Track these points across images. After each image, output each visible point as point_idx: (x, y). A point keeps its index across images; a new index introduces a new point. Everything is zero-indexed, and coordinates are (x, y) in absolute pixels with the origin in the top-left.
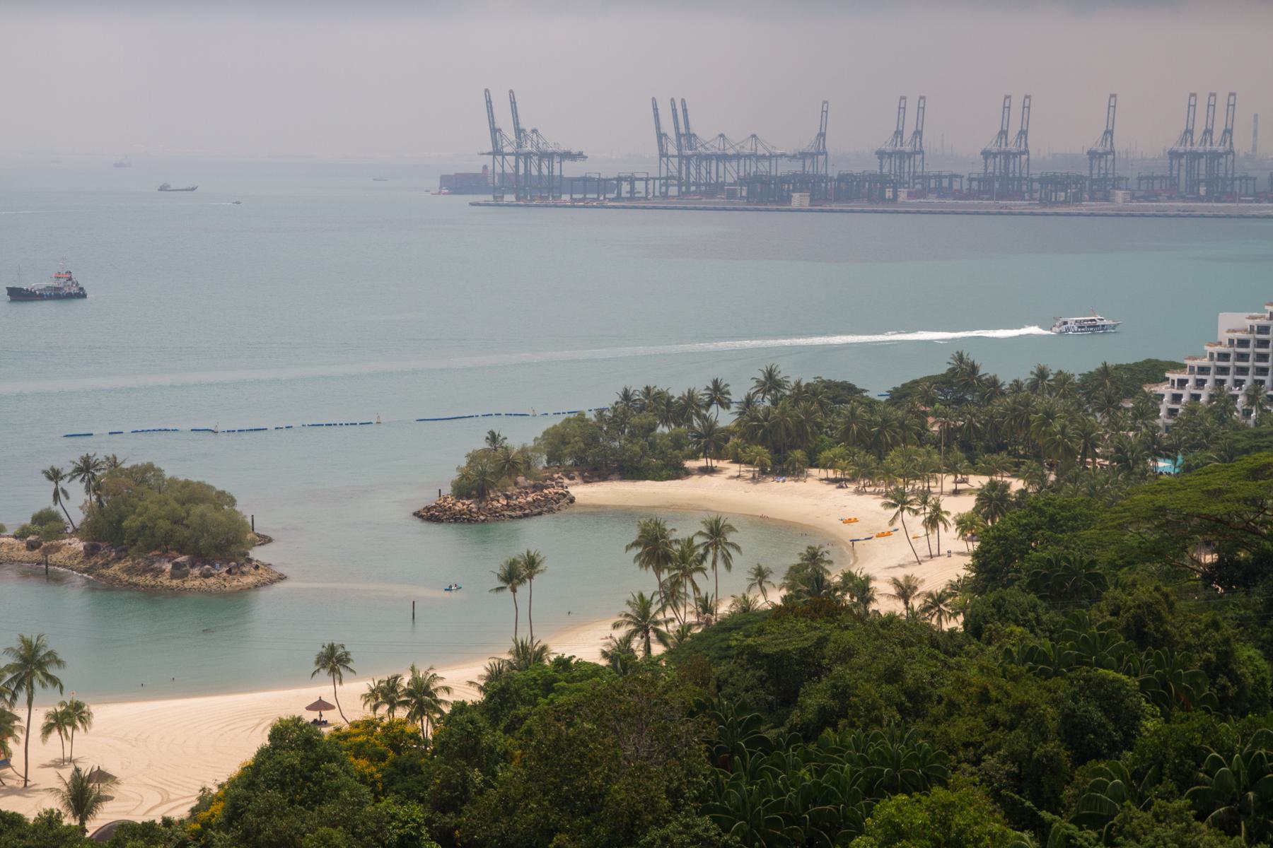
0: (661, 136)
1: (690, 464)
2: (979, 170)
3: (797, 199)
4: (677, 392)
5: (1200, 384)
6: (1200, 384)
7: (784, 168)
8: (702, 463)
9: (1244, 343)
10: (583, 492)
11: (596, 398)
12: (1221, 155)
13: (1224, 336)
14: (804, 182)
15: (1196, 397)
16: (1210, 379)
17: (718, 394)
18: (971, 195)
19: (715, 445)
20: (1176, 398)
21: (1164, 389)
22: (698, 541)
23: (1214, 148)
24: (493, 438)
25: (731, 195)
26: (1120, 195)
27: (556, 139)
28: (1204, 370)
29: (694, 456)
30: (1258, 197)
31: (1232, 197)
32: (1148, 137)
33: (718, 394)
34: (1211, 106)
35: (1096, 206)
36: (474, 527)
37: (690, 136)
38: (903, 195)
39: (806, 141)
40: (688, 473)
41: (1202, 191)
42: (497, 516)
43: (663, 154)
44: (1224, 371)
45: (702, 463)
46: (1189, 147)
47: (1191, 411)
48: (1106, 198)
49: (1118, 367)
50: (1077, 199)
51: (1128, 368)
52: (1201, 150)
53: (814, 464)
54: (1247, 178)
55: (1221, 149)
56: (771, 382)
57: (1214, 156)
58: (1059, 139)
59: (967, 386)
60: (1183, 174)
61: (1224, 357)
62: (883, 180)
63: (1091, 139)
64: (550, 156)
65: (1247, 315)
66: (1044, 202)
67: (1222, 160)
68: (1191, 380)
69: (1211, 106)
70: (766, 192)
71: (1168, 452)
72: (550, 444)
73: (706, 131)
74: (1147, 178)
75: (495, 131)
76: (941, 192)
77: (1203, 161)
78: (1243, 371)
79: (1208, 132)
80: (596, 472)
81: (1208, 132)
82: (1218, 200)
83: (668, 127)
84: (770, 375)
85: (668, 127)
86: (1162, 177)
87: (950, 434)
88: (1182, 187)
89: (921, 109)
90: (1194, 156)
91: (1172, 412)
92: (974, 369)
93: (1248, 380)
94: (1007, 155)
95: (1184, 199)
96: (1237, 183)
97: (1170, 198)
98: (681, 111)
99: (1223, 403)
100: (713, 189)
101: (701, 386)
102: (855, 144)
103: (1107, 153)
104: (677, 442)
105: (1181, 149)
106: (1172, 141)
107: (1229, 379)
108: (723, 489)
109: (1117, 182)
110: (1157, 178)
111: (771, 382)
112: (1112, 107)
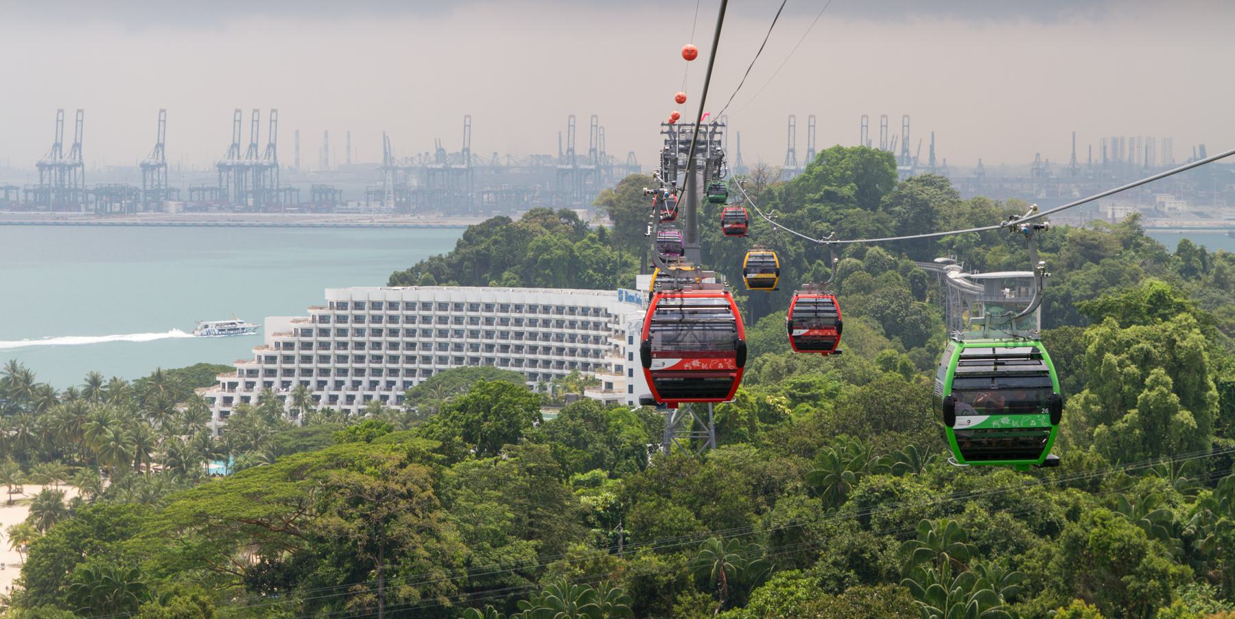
2: (35, 181)
5: (250, 386)
6: (250, 386)
9: (289, 346)
12: (266, 168)
13: (271, 340)
15: (246, 399)
16: (259, 381)
18: (26, 206)
21: (215, 392)
23: (260, 161)
26: (172, 206)
28: (252, 373)
30: (302, 208)
31: (278, 207)
32: (197, 152)
34: (255, 122)
35: (150, 216)
41: (250, 201)
44: (272, 373)
46: (254, 160)
47: (242, 413)
48: (160, 209)
49: (170, 372)
50: (132, 210)
51: (181, 373)
52: (247, 162)
54: (291, 190)
55: (266, 162)
57: (260, 169)
58: (113, 152)
59: (22, 395)
60: (232, 186)
61: (271, 359)
65: (292, 318)
66: (98, 213)
67: (268, 173)
69: (255, 122)
71: (219, 454)
74: (198, 189)
77: (250, 173)
78: (289, 372)
79: (254, 146)
81: (254, 146)
82: (265, 211)
86: (212, 189)
88: (231, 199)
89: (79, 122)
90: (242, 169)
91: (224, 415)
92: (28, 379)
93: (295, 381)
94: (63, 167)
95: (233, 209)
96: (282, 194)
97: (220, 209)
99: (270, 406)
103: (271, 166)
105: (229, 162)
106: (220, 153)
107: (277, 381)
109: (169, 193)
110: (207, 189)
112: (162, 122)
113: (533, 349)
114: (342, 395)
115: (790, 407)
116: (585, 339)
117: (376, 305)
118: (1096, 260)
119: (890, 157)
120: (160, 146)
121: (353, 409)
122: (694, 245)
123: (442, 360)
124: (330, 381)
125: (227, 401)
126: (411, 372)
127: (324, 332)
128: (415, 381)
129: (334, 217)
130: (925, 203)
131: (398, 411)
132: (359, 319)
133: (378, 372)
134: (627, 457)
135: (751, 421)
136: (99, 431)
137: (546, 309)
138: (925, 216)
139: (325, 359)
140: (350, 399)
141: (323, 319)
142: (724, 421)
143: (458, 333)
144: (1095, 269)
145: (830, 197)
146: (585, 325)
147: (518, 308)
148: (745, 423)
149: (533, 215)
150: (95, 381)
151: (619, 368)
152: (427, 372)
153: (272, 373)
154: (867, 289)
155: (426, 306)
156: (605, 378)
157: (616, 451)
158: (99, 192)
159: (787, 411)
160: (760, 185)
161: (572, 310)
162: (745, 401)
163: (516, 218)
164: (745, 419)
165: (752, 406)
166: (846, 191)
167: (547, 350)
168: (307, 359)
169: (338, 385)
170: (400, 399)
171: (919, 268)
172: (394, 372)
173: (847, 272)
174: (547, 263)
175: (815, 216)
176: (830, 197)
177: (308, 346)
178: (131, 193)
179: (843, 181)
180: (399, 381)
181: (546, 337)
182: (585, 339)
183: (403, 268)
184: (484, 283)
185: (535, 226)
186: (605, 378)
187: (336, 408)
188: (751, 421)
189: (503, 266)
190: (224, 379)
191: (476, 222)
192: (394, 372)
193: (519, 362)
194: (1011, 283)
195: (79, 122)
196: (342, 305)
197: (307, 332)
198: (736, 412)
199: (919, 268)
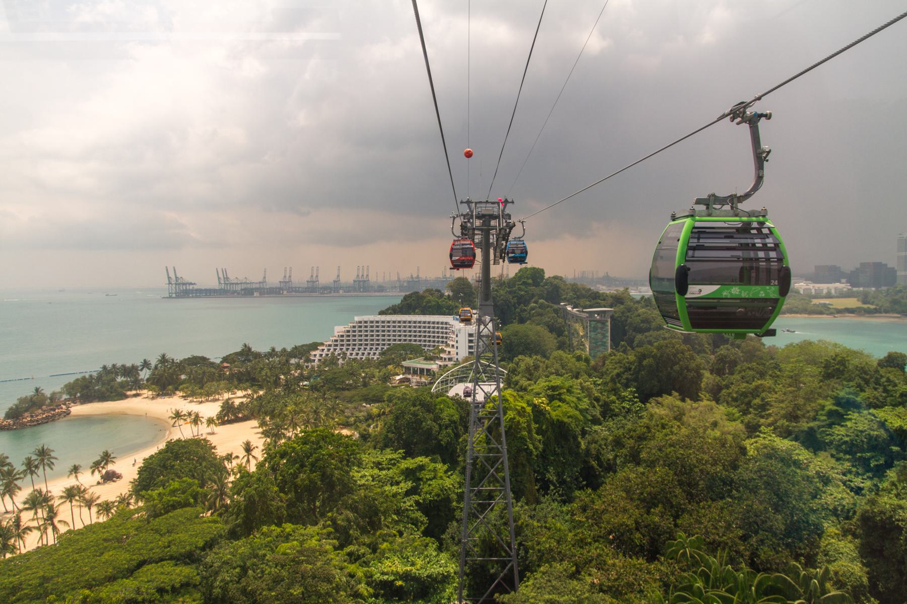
0: (219, 278)
1: (129, 393)
2: (279, 286)
3: (255, 294)
4: (239, 349)
6: (329, 350)
7: (254, 286)
8: (134, 392)
9: (342, 336)
10: (77, 409)
11: (92, 368)
13: (336, 334)
14: (257, 289)
16: (332, 349)
17: (146, 364)
18: (305, 292)
19: (137, 385)
20: (321, 355)
21: (318, 353)
22: (34, 457)
24: (37, 390)
25: (238, 294)
27: (187, 279)
28: (330, 345)
29: (131, 390)
30: (375, 291)
31: (368, 291)
32: (348, 277)
33: (146, 364)
36: (12, 432)
37: (227, 278)
38: (285, 292)
39: (260, 279)
40: (127, 397)
42: (23, 426)
43: (220, 283)
44: (336, 345)
45: (134, 392)
51: (306, 345)
53: (177, 389)
56: (163, 360)
58: (325, 279)
61: (336, 341)
62: (281, 289)
63: (334, 278)
64: (184, 284)
66: (322, 293)
68: (326, 349)
70: (248, 292)
71: (308, 379)
73: (232, 277)
75: (169, 278)
76: (296, 291)
80: (87, 398)
83: (221, 276)
84: (163, 356)
85: (221, 276)
87: (232, 376)
89: (317, 270)
91: (320, 360)
92: (250, 349)
94: (313, 282)
98: (225, 272)
100: (235, 292)
101: (138, 363)
102: (274, 280)
104: (122, 385)
107: (344, 348)
108: (142, 404)
109: (340, 288)
111: (163, 360)
113: (425, 336)
114: (360, 353)
115: (548, 405)
116: (442, 333)
117: (372, 322)
118: (622, 303)
119: (542, 270)
120: (338, 276)
121: (364, 357)
122: (488, 303)
123: (395, 340)
124: (356, 348)
125: (321, 355)
126: (384, 345)
127: (354, 331)
128: (385, 348)
129: (383, 294)
130: (556, 285)
131: (142, 516)
132: (366, 327)
133: (372, 345)
134: (446, 428)
135: (529, 426)
136: (260, 372)
137: (429, 323)
138: (556, 288)
139: (354, 340)
140: (363, 354)
141: (354, 327)
142: (510, 427)
143: (400, 331)
144: (622, 307)
145: (524, 283)
146: (442, 328)
147: (420, 322)
148: (524, 428)
149: (427, 291)
150: (273, 350)
151: (453, 346)
152: (389, 344)
153: (336, 345)
154: (541, 315)
155: (389, 322)
156: (448, 349)
157: (440, 425)
158: (322, 288)
159: (548, 408)
160: (501, 280)
161: (438, 323)
162: (524, 412)
163: (421, 292)
164: (525, 425)
165: (529, 416)
166: (530, 281)
167: (429, 337)
168: (349, 340)
169: (359, 349)
170: (380, 354)
171: (556, 307)
172: (378, 345)
173: (533, 309)
174: (430, 307)
175: (520, 289)
176: (524, 283)
177: (349, 336)
178: (330, 288)
179: (528, 278)
180: (380, 347)
181: (429, 332)
182: (442, 333)
183: (384, 309)
184: (410, 314)
185: (427, 294)
186: (448, 349)
187: (358, 357)
188: (529, 426)
189: (416, 308)
190: (320, 348)
191: (408, 293)
192: (378, 345)
193: (420, 341)
194: (598, 313)
195: (317, 270)
196: (360, 322)
197: (348, 331)
198: (519, 422)
199: (556, 307)
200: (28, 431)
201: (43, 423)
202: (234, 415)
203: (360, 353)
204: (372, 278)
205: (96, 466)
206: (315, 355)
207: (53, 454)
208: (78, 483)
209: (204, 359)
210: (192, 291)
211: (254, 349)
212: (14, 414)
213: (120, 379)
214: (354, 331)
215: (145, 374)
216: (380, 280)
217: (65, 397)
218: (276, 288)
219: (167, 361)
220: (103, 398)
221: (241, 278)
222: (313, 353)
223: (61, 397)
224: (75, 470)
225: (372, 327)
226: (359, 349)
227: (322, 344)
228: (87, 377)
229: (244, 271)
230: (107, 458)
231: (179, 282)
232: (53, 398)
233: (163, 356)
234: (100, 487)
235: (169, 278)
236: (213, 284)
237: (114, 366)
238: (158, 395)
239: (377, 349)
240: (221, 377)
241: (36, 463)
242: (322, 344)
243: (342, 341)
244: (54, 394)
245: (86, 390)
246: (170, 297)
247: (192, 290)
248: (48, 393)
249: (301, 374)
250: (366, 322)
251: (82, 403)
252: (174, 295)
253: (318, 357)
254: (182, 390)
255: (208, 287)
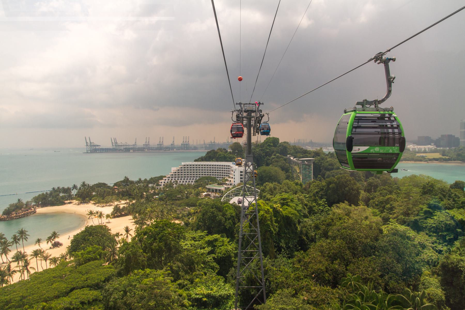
0: (112, 143)
1: (66, 202)
2: (143, 147)
3: (131, 151)
4: (122, 179)
6: (168, 180)
7: (130, 147)
8: (69, 201)
9: (175, 172)
10: (40, 210)
11: (47, 189)
13: (172, 172)
14: (132, 148)
16: (170, 179)
17: (75, 187)
18: (156, 150)
19: (70, 197)
20: (165, 182)
21: (163, 181)
22: (17, 235)
24: (19, 200)
25: (122, 151)
27: (96, 143)
28: (169, 177)
29: (67, 200)
30: (192, 149)
31: (189, 149)
32: (179, 142)
33: (75, 187)
36: (6, 222)
37: (117, 143)
38: (146, 150)
39: (134, 143)
40: (65, 204)
42: (12, 219)
43: (113, 145)
44: (172, 177)
45: (69, 201)
51: (157, 177)
53: (91, 200)
56: (84, 185)
58: (167, 143)
61: (172, 175)
62: (144, 148)
63: (171, 143)
64: (94, 146)
66: (165, 151)
68: (167, 179)
70: (127, 150)
71: (158, 194)
72: (374, 142)
73: (119, 142)
75: (87, 143)
76: (152, 150)
80: (44, 205)
83: (113, 141)
84: (84, 183)
85: (113, 141)
87: (119, 193)
89: (163, 139)
91: (164, 185)
92: (128, 179)
94: (161, 145)
98: (115, 139)
100: (121, 150)
101: (71, 186)
102: (140, 144)
104: (63, 198)
107: (177, 179)
108: (73, 207)
109: (175, 148)
111: (84, 185)
113: (218, 173)
114: (185, 181)
115: (281, 208)
116: (227, 171)
117: (191, 165)
118: (319, 156)
119: (278, 139)
120: (173, 142)
121: (187, 183)
122: (250, 155)
123: (202, 175)
124: (183, 178)
125: (165, 182)
126: (197, 177)
127: (182, 170)
128: (198, 178)
129: (197, 151)
130: (285, 146)
131: (73, 265)
132: (188, 168)
133: (191, 177)
134: (229, 220)
135: (271, 219)
136: (133, 191)
137: (220, 166)
138: (285, 148)
139: (182, 175)
140: (186, 182)
141: (182, 168)
142: (262, 219)
143: (205, 170)
144: (319, 157)
145: (269, 145)
146: (227, 168)
147: (215, 165)
148: (269, 220)
149: (219, 149)
150: (140, 179)
151: (232, 177)
152: (200, 177)
153: (172, 177)
154: (277, 162)
155: (199, 165)
156: (230, 179)
157: (225, 218)
158: (165, 148)
159: (281, 209)
160: (257, 144)
161: (224, 166)
162: (269, 211)
163: (216, 150)
164: (269, 218)
165: (271, 213)
166: (272, 144)
167: (220, 173)
168: (179, 175)
169: (184, 179)
170: (195, 182)
171: (285, 157)
172: (194, 177)
173: (273, 158)
174: (220, 158)
175: (267, 148)
176: (269, 145)
177: (179, 172)
178: (169, 148)
179: (271, 143)
180: (195, 178)
181: (220, 170)
182: (227, 171)
183: (197, 159)
184: (210, 161)
185: (219, 151)
186: (230, 179)
187: (184, 183)
188: (271, 219)
189: (213, 158)
190: (164, 179)
191: (209, 151)
192: (194, 177)
193: (215, 175)
194: (307, 161)
195: (163, 139)
196: (185, 165)
197: (179, 170)
198: (266, 216)
199: (285, 157)
200: (14, 221)
201: (22, 217)
202: (120, 213)
203: (185, 181)
204: (191, 143)
205: (49, 239)
206: (162, 182)
207: (27, 233)
208: (40, 248)
209: (104, 184)
210: (99, 149)
211: (130, 179)
212: (7, 212)
213: (61, 195)
214: (182, 170)
215: (74, 192)
216: (195, 144)
217: (33, 204)
218: (142, 148)
219: (86, 185)
220: (53, 204)
221: (124, 143)
222: (161, 181)
223: (31, 204)
224: (39, 241)
225: (191, 168)
226: (184, 179)
227: (165, 177)
228: (45, 193)
229: (125, 139)
230: (55, 235)
231: (92, 145)
232: (27, 204)
233: (84, 183)
234: (51, 250)
235: (87, 143)
236: (109, 146)
237: (58, 188)
238: (81, 203)
239: (193, 179)
240: (113, 193)
241: (19, 238)
242: (165, 177)
243: (175, 175)
244: (28, 202)
245: (44, 200)
246: (87, 152)
247: (99, 149)
248: (24, 201)
249: (154, 192)
250: (188, 165)
251: (42, 207)
252: (89, 152)
253: (163, 183)
254: (93, 200)
255: (107, 147)
